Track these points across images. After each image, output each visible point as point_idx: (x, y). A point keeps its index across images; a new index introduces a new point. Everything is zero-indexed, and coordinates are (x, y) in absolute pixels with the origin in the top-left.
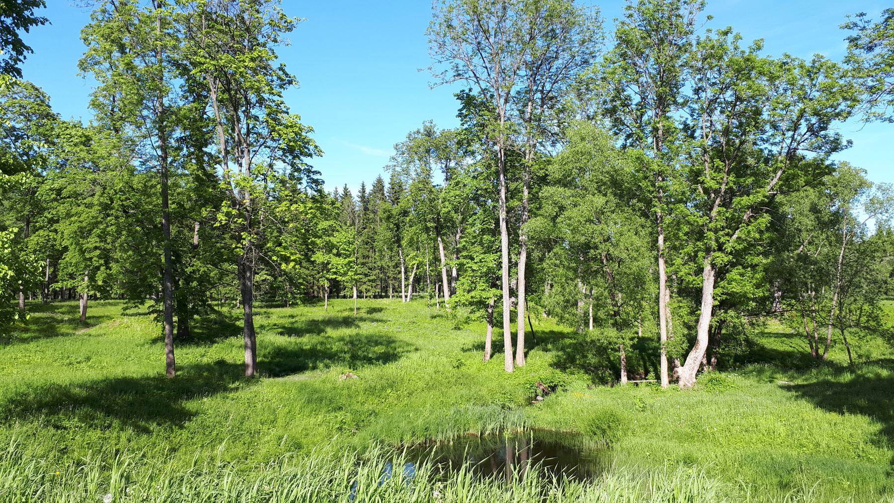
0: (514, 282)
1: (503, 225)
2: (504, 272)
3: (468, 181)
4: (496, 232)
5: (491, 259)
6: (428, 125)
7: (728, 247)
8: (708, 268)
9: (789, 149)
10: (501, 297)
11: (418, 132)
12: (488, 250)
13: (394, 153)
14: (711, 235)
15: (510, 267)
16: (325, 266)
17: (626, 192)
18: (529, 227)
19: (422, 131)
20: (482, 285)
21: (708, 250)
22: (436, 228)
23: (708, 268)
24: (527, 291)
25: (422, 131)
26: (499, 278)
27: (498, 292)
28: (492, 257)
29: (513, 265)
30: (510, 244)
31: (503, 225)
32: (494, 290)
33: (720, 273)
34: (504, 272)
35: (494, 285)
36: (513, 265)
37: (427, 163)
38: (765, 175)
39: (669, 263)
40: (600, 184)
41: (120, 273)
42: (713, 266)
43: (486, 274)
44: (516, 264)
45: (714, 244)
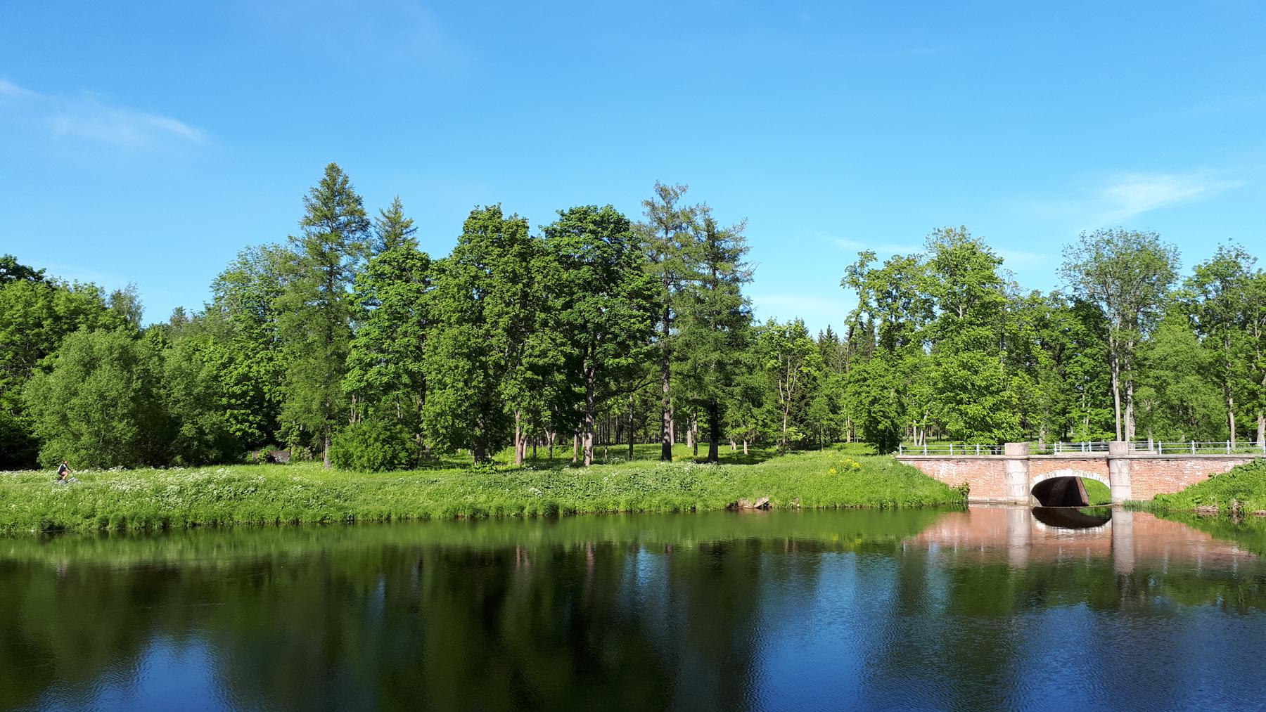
2: (1118, 421)
39: (1236, 415)
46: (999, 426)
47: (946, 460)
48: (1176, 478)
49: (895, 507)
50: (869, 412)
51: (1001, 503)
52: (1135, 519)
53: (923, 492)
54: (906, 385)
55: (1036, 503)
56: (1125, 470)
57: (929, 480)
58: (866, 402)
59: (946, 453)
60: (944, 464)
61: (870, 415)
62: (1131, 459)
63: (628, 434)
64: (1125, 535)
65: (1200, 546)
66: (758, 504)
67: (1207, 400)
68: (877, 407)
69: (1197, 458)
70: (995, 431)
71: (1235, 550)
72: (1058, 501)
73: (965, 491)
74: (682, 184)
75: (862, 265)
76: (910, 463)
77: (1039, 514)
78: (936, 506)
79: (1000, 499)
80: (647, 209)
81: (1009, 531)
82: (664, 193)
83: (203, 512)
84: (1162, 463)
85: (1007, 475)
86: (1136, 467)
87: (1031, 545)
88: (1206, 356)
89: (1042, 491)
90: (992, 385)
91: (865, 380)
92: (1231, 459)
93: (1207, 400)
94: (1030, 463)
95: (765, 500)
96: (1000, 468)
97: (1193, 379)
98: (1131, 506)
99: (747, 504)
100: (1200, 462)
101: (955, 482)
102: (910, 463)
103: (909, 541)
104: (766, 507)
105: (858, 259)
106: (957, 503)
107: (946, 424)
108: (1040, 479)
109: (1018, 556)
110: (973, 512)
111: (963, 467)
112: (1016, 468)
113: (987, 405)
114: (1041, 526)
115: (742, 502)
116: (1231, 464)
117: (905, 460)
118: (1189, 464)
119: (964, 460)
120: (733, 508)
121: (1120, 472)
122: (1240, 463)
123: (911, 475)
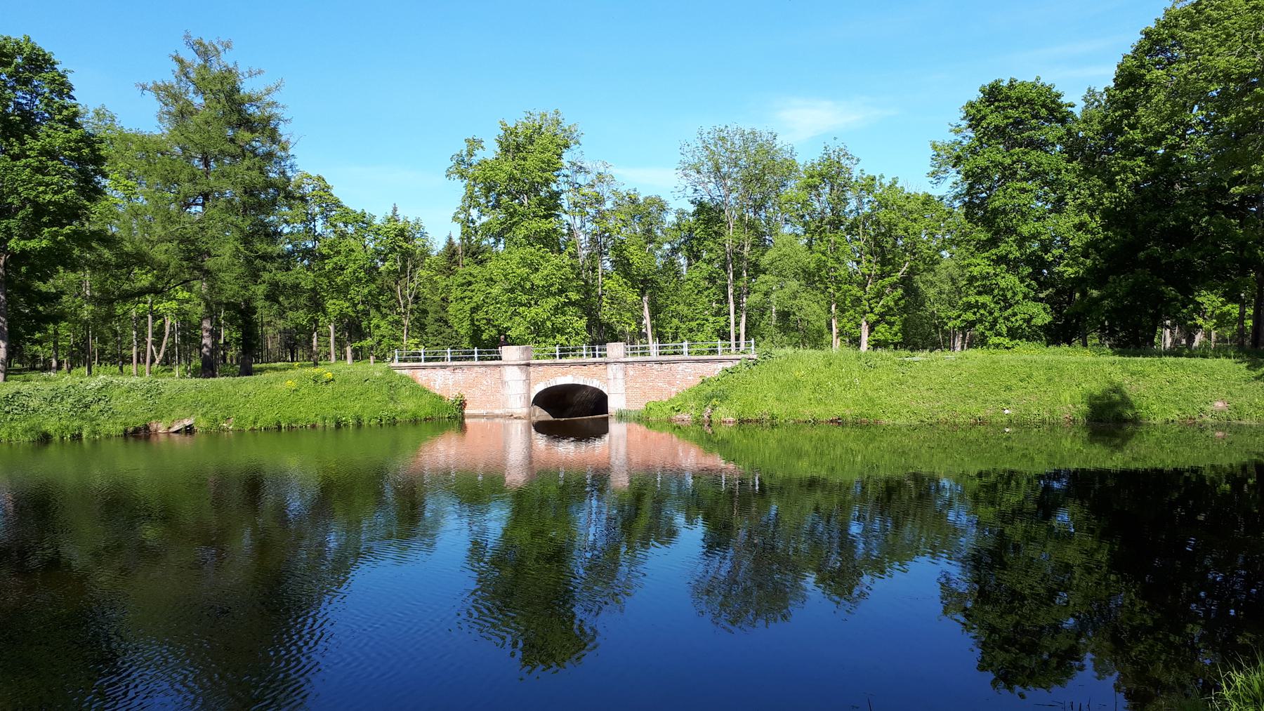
1: (731, 298)
2: (732, 328)
7: (876, 310)
9: (205, 299)
12: (718, 313)
14: (865, 302)
16: (1159, 659)
17: (810, 277)
21: (865, 312)
23: (864, 324)
28: (722, 319)
29: (737, 324)
30: (736, 309)
31: (731, 298)
33: (872, 329)
36: (737, 324)
38: (899, 265)
39: (839, 321)
40: (796, 274)
46: (561, 331)
47: (442, 367)
48: (669, 383)
49: (359, 424)
50: (472, 320)
52: (629, 430)
53: (408, 405)
55: (542, 415)
56: (620, 375)
57: (419, 391)
58: (467, 308)
60: (441, 372)
61: (473, 324)
62: (626, 363)
63: (99, 346)
64: (617, 447)
65: (691, 458)
66: (176, 428)
67: (811, 308)
68: (481, 315)
69: (688, 361)
70: (558, 336)
71: (716, 461)
72: (571, 412)
73: (462, 404)
74: (224, 39)
75: (470, 154)
76: (405, 372)
78: (415, 421)
79: (497, 412)
80: (176, 67)
81: (504, 451)
82: (204, 51)
83: (422, 414)
84: (656, 366)
85: (504, 383)
88: (810, 260)
90: (552, 285)
91: (470, 283)
92: (720, 361)
93: (811, 308)
94: (531, 369)
95: (187, 422)
96: (497, 376)
97: (794, 284)
99: (162, 428)
100: (700, 365)
101: (451, 395)
102: (405, 372)
103: (402, 466)
104: (189, 430)
105: (464, 148)
106: (453, 417)
107: (508, 329)
108: (539, 387)
109: (516, 477)
111: (459, 375)
112: (513, 376)
113: (547, 307)
115: (154, 426)
116: (720, 366)
117: (400, 368)
118: (681, 367)
120: (140, 434)
122: (729, 365)
123: (392, 387)
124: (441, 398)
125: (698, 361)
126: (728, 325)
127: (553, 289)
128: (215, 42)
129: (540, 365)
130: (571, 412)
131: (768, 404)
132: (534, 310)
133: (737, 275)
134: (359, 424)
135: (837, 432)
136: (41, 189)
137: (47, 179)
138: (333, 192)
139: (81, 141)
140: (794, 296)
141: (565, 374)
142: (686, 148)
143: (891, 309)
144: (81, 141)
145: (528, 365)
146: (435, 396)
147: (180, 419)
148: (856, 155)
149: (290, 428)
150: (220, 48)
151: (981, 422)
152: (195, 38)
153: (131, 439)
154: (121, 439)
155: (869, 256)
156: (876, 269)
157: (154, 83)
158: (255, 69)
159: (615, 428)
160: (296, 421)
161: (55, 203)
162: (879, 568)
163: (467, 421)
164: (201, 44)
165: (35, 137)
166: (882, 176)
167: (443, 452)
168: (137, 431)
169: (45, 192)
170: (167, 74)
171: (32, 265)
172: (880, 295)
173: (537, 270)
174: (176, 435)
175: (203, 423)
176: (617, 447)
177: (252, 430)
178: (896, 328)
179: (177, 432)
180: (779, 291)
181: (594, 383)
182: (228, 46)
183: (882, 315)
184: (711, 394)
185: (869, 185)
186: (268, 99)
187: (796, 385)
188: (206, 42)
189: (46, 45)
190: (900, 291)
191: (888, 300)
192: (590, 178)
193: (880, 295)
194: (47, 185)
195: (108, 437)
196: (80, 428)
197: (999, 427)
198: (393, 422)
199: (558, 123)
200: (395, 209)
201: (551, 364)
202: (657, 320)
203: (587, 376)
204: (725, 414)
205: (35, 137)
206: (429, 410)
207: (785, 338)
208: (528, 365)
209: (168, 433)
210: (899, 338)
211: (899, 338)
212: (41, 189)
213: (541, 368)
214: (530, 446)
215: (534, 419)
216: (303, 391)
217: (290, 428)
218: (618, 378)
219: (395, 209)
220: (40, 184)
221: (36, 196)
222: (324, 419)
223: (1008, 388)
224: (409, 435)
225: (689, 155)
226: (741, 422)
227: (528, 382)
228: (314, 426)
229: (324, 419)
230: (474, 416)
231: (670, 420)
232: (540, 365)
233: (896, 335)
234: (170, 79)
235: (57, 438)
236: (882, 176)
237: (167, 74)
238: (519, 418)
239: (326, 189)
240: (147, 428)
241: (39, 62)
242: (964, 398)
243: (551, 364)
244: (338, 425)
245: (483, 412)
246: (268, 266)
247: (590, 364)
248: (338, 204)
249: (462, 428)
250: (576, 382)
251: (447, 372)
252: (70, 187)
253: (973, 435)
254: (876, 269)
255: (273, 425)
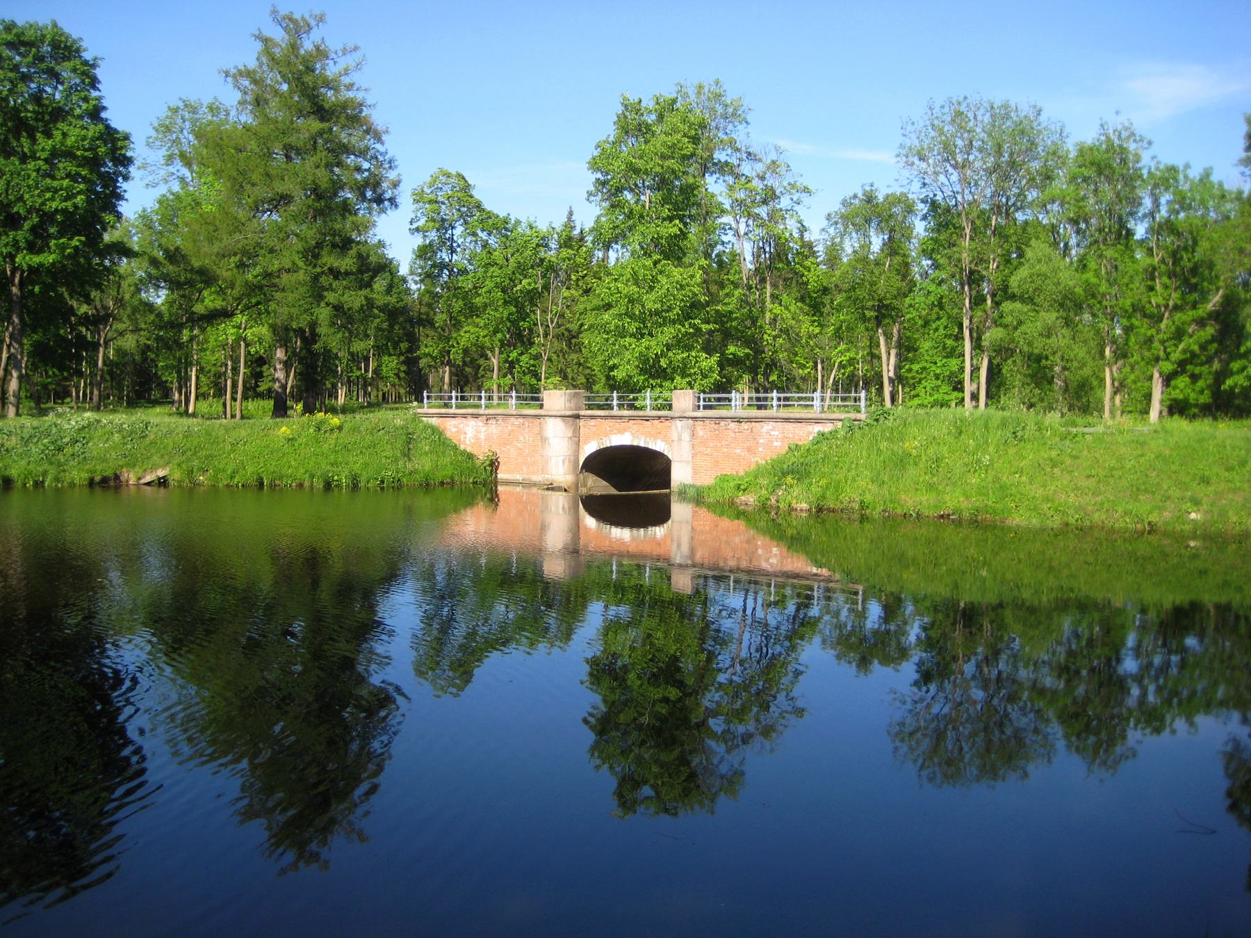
0: (975, 386)
1: (966, 333)
2: (967, 375)
3: (932, 288)
4: (959, 338)
5: (954, 363)
6: (868, 189)
8: (1156, 375)
10: (963, 399)
11: (855, 196)
13: (825, 223)
15: (972, 372)
18: (992, 335)
19: (860, 195)
20: (945, 388)
21: (1157, 359)
22: (877, 317)
23: (1156, 375)
24: (988, 396)
25: (860, 195)
26: (961, 382)
27: (960, 395)
29: (975, 370)
30: (973, 349)
31: (966, 333)
32: (956, 394)
33: (1168, 380)
34: (967, 375)
35: (955, 389)
36: (975, 370)
37: (866, 236)
41: (754, 380)
42: (1161, 374)
43: (950, 377)
44: (978, 369)
45: (1162, 354)
48: (749, 450)
49: (355, 486)
51: (535, 484)
53: (423, 463)
54: (366, 298)
55: (598, 486)
56: (686, 436)
59: (446, 406)
60: (472, 422)
66: (148, 479)
69: (739, 420)
72: (630, 486)
73: (494, 464)
74: (317, 12)
77: (599, 507)
78: (427, 486)
79: (535, 478)
80: (259, 46)
81: (543, 528)
82: (296, 28)
83: (439, 476)
84: (733, 425)
85: (544, 440)
86: (701, 429)
87: (573, 550)
89: (608, 463)
90: (670, 309)
92: (817, 421)
94: (582, 423)
95: (161, 473)
96: (536, 430)
98: (698, 498)
99: (130, 477)
101: (482, 454)
104: (163, 482)
106: (481, 483)
108: (590, 448)
110: (502, 497)
111: (494, 428)
112: (556, 432)
114: (590, 522)
115: (124, 477)
116: (818, 428)
118: (767, 427)
119: (495, 416)
120: (108, 484)
121: (680, 439)
122: (827, 428)
124: (470, 456)
125: (787, 420)
126: (962, 369)
127: (672, 315)
128: (307, 17)
129: (592, 417)
130: (630, 486)
131: (860, 488)
132: (645, 342)
133: (978, 301)
134: (355, 486)
135: (950, 535)
136: (48, 195)
137: (55, 184)
138: (474, 193)
139: (98, 139)
140: (1048, 333)
141: (621, 432)
142: (910, 128)
143: (1193, 355)
144: (98, 139)
145: (577, 417)
146: (464, 453)
147: (154, 468)
148: (1148, 136)
149: (273, 486)
150: (313, 23)
151: (1153, 529)
152: (284, 11)
153: (98, 489)
154: (86, 490)
155: (1165, 280)
156: (1175, 297)
157: (236, 67)
158: (351, 45)
159: (679, 510)
160: (281, 478)
161: (64, 211)
162: (1153, 719)
163: (499, 488)
164: (290, 19)
165: (48, 135)
166: (1187, 166)
167: (473, 527)
168: (105, 480)
169: (53, 199)
170: (249, 57)
171: (43, 283)
172: (1179, 335)
173: (652, 288)
174: (148, 488)
175: (177, 475)
176: (679, 535)
177: (228, 486)
178: (1201, 384)
179: (148, 484)
180: (1036, 326)
181: (658, 446)
182: (321, 19)
183: (1182, 364)
184: (793, 469)
185: (1167, 178)
186: (346, 80)
187: (901, 462)
188: (297, 16)
189: (73, 29)
190: (1210, 331)
191: (1190, 343)
192: (760, 167)
193: (1179, 335)
194: (56, 191)
195: (72, 485)
196: (45, 473)
197: (1180, 538)
198: (397, 486)
199: (718, 96)
200: (571, 213)
201: (606, 417)
202: (674, 370)
203: (648, 434)
204: (800, 499)
205: (48, 135)
206: (449, 471)
207: (1037, 391)
208: (577, 417)
209: (138, 485)
210: (1205, 398)
211: (1205, 398)
212: (48, 195)
213: (593, 422)
214: (576, 526)
215: (583, 491)
216: (303, 440)
217: (273, 486)
218: (702, 443)
219: (571, 213)
220: (48, 189)
221: (43, 204)
222: (312, 476)
223: (1205, 481)
224: (424, 503)
225: (914, 136)
226: (820, 510)
227: (577, 441)
228: (301, 485)
229: (312, 476)
230: (507, 483)
231: (732, 503)
232: (592, 417)
233: (1202, 392)
234: (252, 64)
235: (20, 483)
236: (1187, 166)
237: (249, 57)
238: (559, 489)
239: (466, 188)
240: (117, 477)
241: (65, 49)
242: (1136, 491)
243: (606, 417)
244: (328, 486)
245: (519, 477)
246: (335, 284)
247: (654, 418)
248: (479, 206)
249: (493, 499)
250: (635, 444)
251: (479, 423)
252: (79, 193)
253: (1142, 548)
254: (1175, 297)
255: (252, 481)
